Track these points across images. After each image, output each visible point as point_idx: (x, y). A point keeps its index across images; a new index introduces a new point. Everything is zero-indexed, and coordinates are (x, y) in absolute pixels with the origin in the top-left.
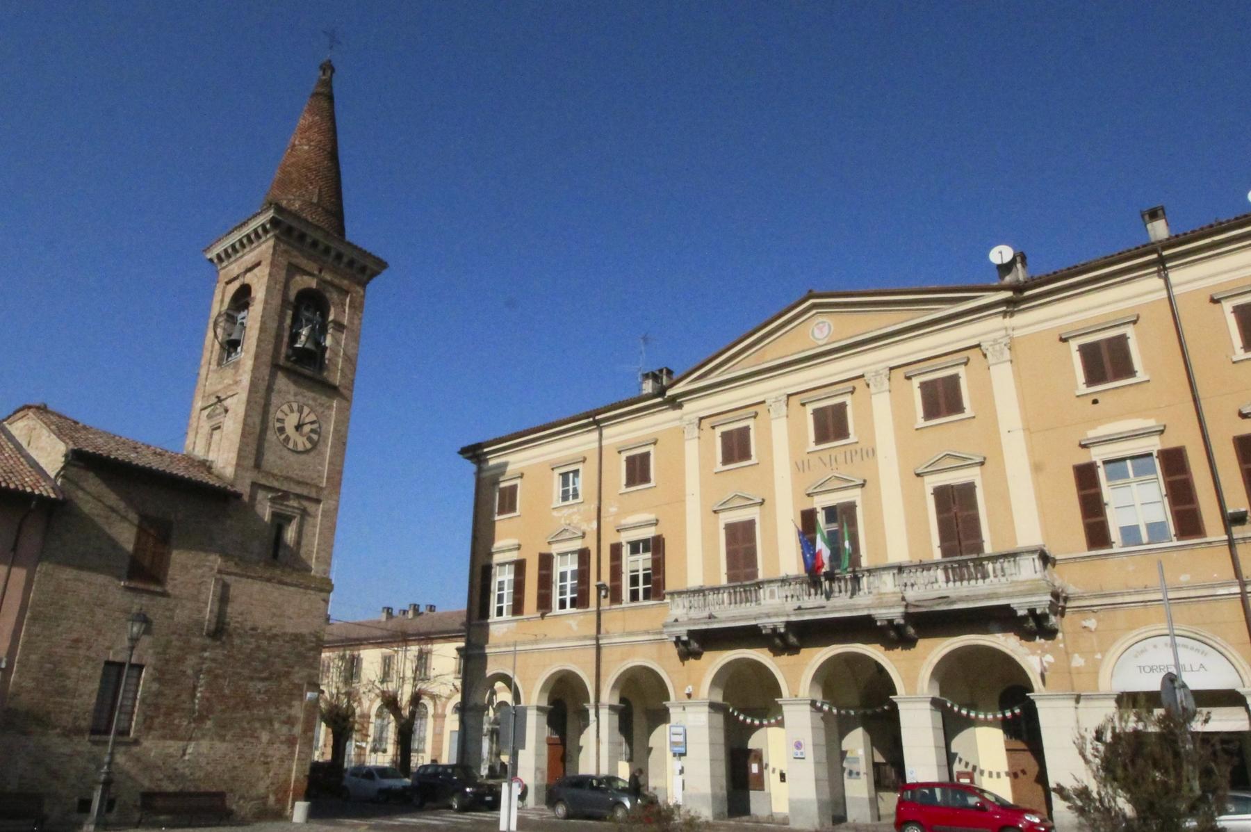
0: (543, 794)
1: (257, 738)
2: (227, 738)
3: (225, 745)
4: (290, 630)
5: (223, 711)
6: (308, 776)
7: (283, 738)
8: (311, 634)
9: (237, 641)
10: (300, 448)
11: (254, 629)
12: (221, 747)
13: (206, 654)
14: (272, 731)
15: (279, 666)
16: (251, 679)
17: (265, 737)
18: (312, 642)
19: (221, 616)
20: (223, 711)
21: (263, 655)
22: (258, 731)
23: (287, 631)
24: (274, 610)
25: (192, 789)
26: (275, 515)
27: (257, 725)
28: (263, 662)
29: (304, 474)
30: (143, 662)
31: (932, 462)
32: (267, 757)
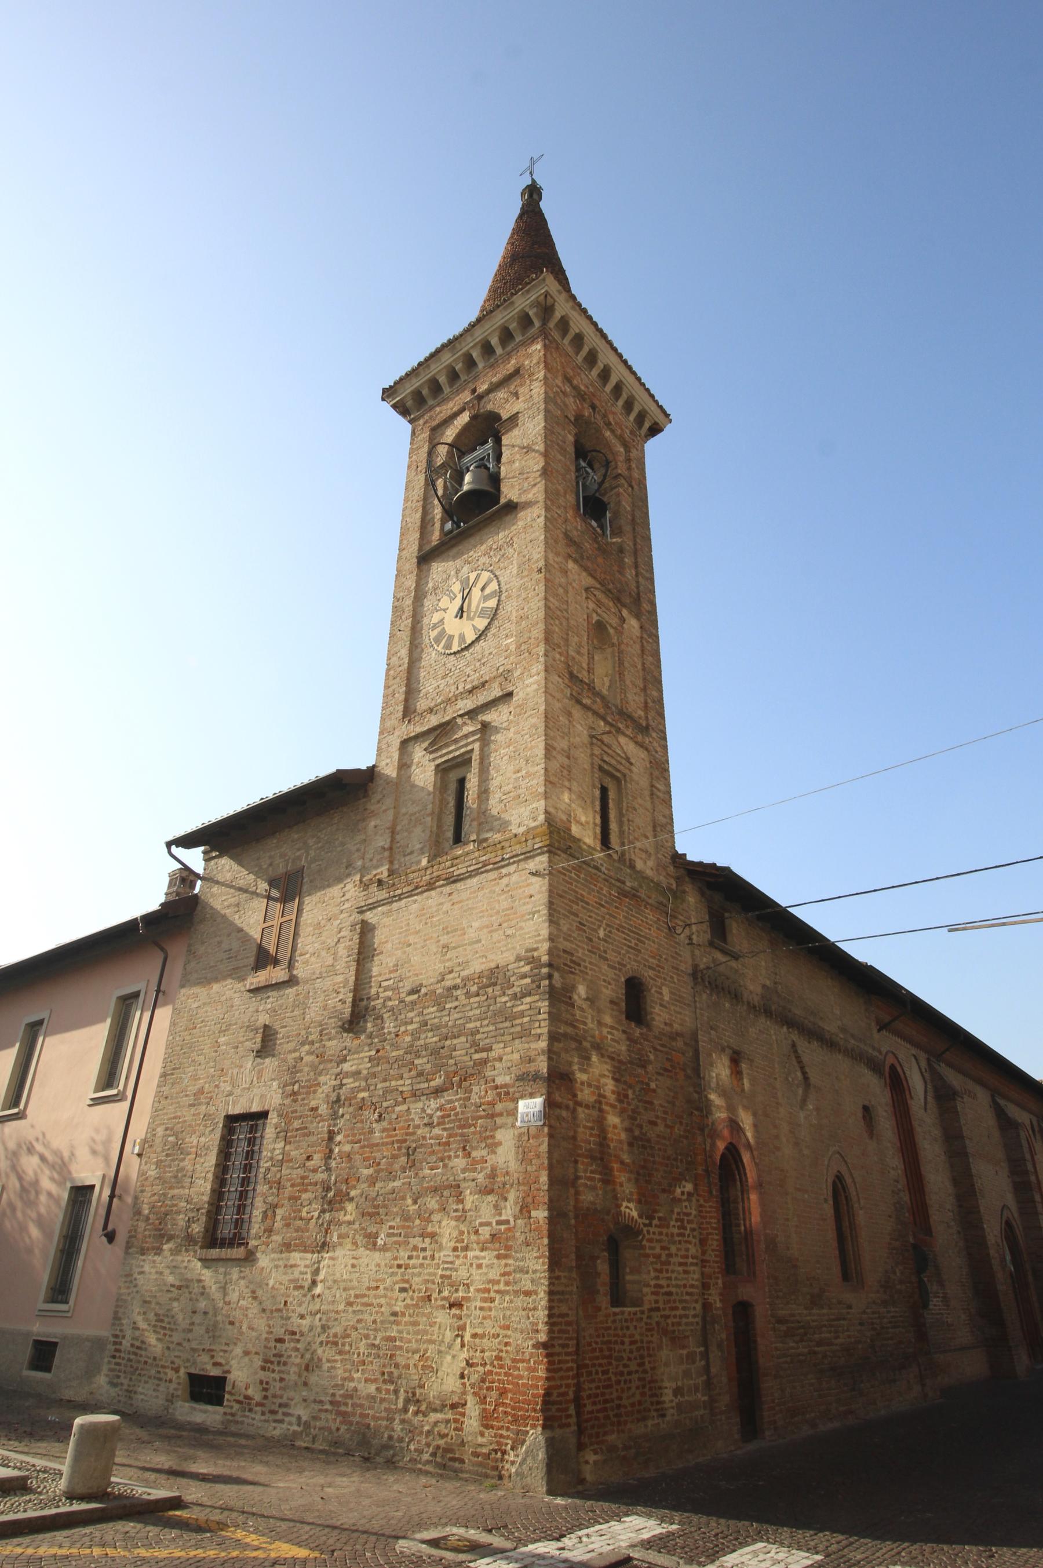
0: (641, 984)
1: (433, 1235)
2: (380, 1242)
3: (377, 1255)
4: (477, 966)
5: (372, 1181)
6: (545, 1345)
7: (485, 1232)
8: (519, 959)
9: (389, 1026)
10: (470, 637)
11: (414, 991)
12: (371, 1260)
13: (346, 1067)
14: (462, 1217)
15: (461, 1052)
16: (415, 1095)
17: (447, 1229)
18: (524, 976)
19: (22, 1186)
20: (372, 1181)
21: (432, 1039)
22: (436, 1217)
23: (453, 1223)
24: (444, 939)
25: (584, 574)
26: (443, 770)
27: (432, 1203)
28: (435, 1052)
29: (484, 547)
30: (266, 1108)
31: (612, 814)
32: (455, 1286)
